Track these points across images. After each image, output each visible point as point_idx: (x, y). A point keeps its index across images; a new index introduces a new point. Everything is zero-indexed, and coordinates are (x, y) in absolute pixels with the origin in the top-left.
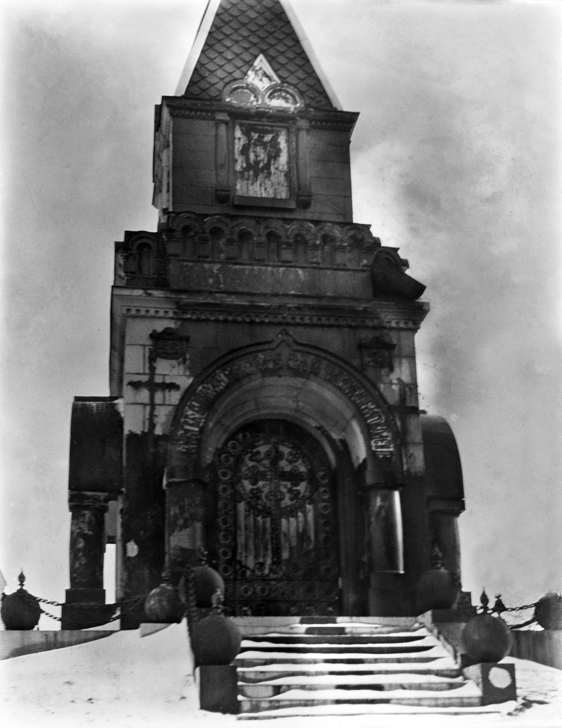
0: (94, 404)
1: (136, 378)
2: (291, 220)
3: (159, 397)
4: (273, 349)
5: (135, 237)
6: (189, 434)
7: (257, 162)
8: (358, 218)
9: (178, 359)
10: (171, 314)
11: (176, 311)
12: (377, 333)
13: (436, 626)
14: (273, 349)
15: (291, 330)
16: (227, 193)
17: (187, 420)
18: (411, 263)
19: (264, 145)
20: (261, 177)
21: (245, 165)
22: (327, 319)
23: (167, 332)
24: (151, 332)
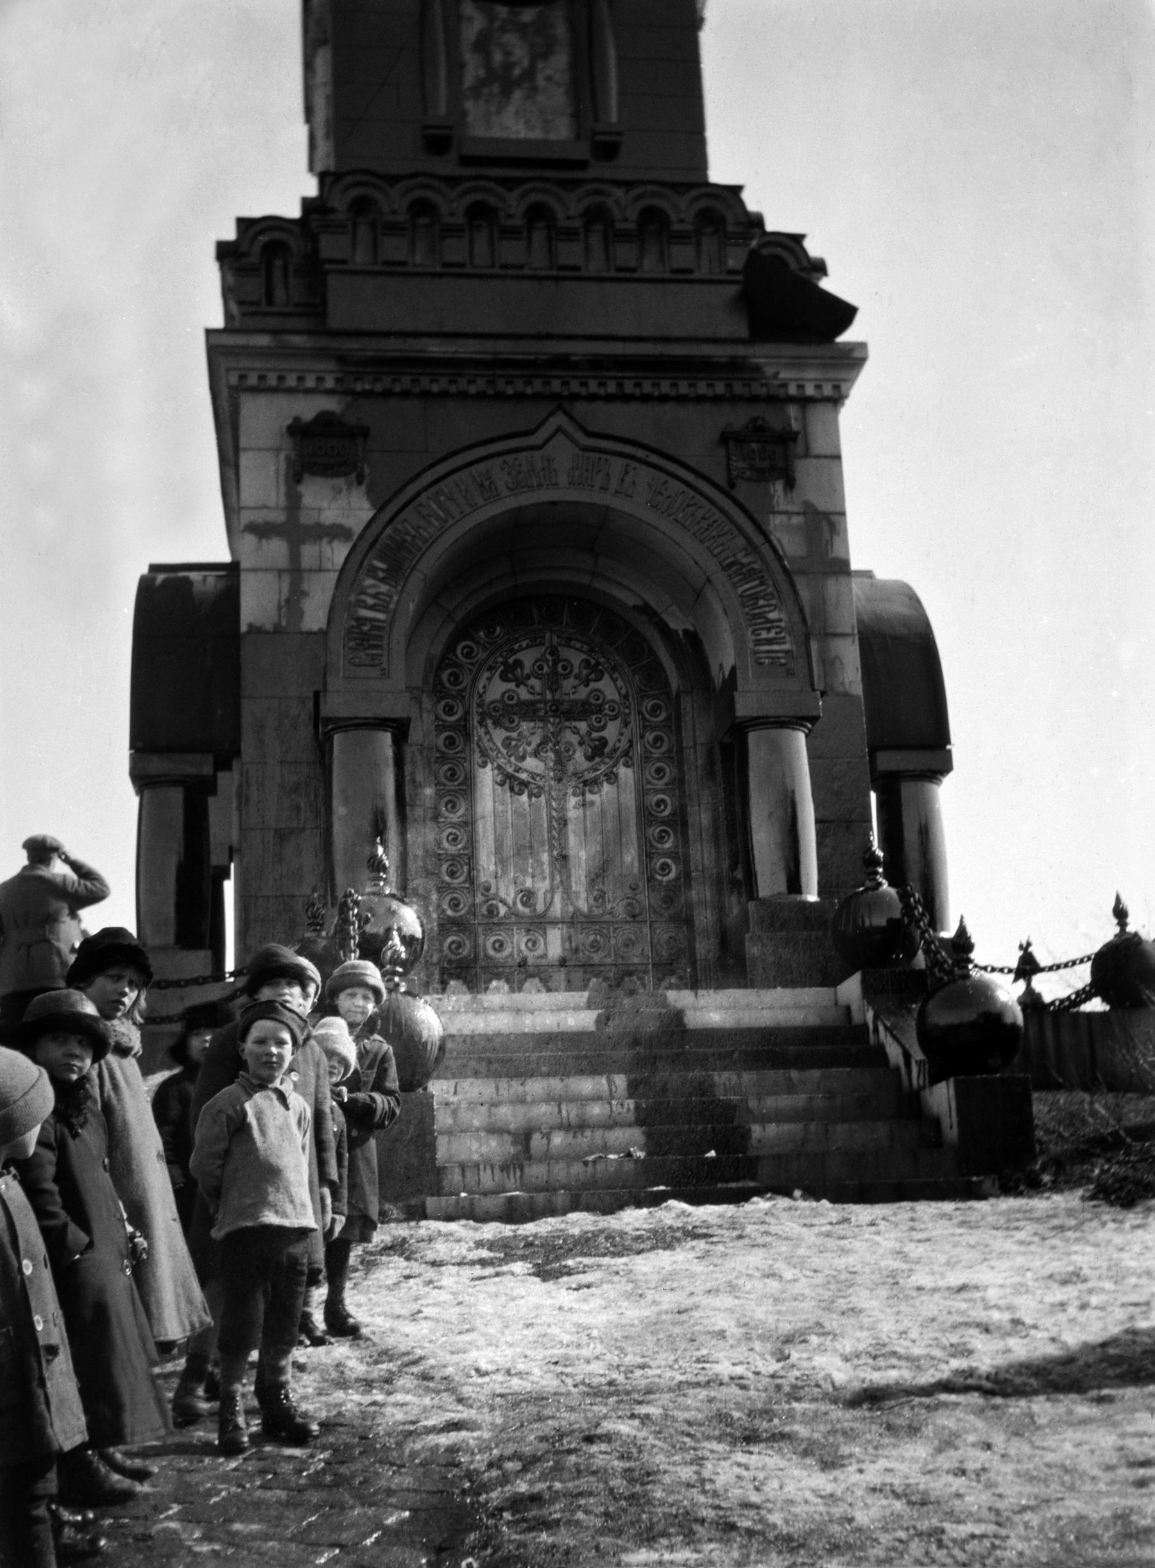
0: (194, 576)
1: (259, 517)
2: (577, 183)
3: (309, 553)
4: (538, 448)
5: (258, 227)
6: (366, 628)
7: (508, 66)
8: (718, 174)
9: (345, 475)
10: (330, 383)
11: (340, 375)
12: (758, 410)
13: (870, 1003)
14: (538, 448)
15: (580, 408)
16: (446, 132)
17: (363, 597)
18: (831, 267)
19: (523, 30)
20: (517, 95)
21: (482, 73)
22: (744, 385)
23: (325, 420)
24: (289, 421)
